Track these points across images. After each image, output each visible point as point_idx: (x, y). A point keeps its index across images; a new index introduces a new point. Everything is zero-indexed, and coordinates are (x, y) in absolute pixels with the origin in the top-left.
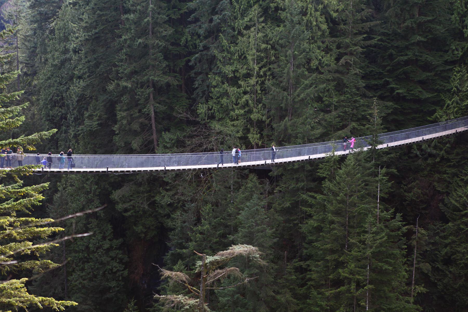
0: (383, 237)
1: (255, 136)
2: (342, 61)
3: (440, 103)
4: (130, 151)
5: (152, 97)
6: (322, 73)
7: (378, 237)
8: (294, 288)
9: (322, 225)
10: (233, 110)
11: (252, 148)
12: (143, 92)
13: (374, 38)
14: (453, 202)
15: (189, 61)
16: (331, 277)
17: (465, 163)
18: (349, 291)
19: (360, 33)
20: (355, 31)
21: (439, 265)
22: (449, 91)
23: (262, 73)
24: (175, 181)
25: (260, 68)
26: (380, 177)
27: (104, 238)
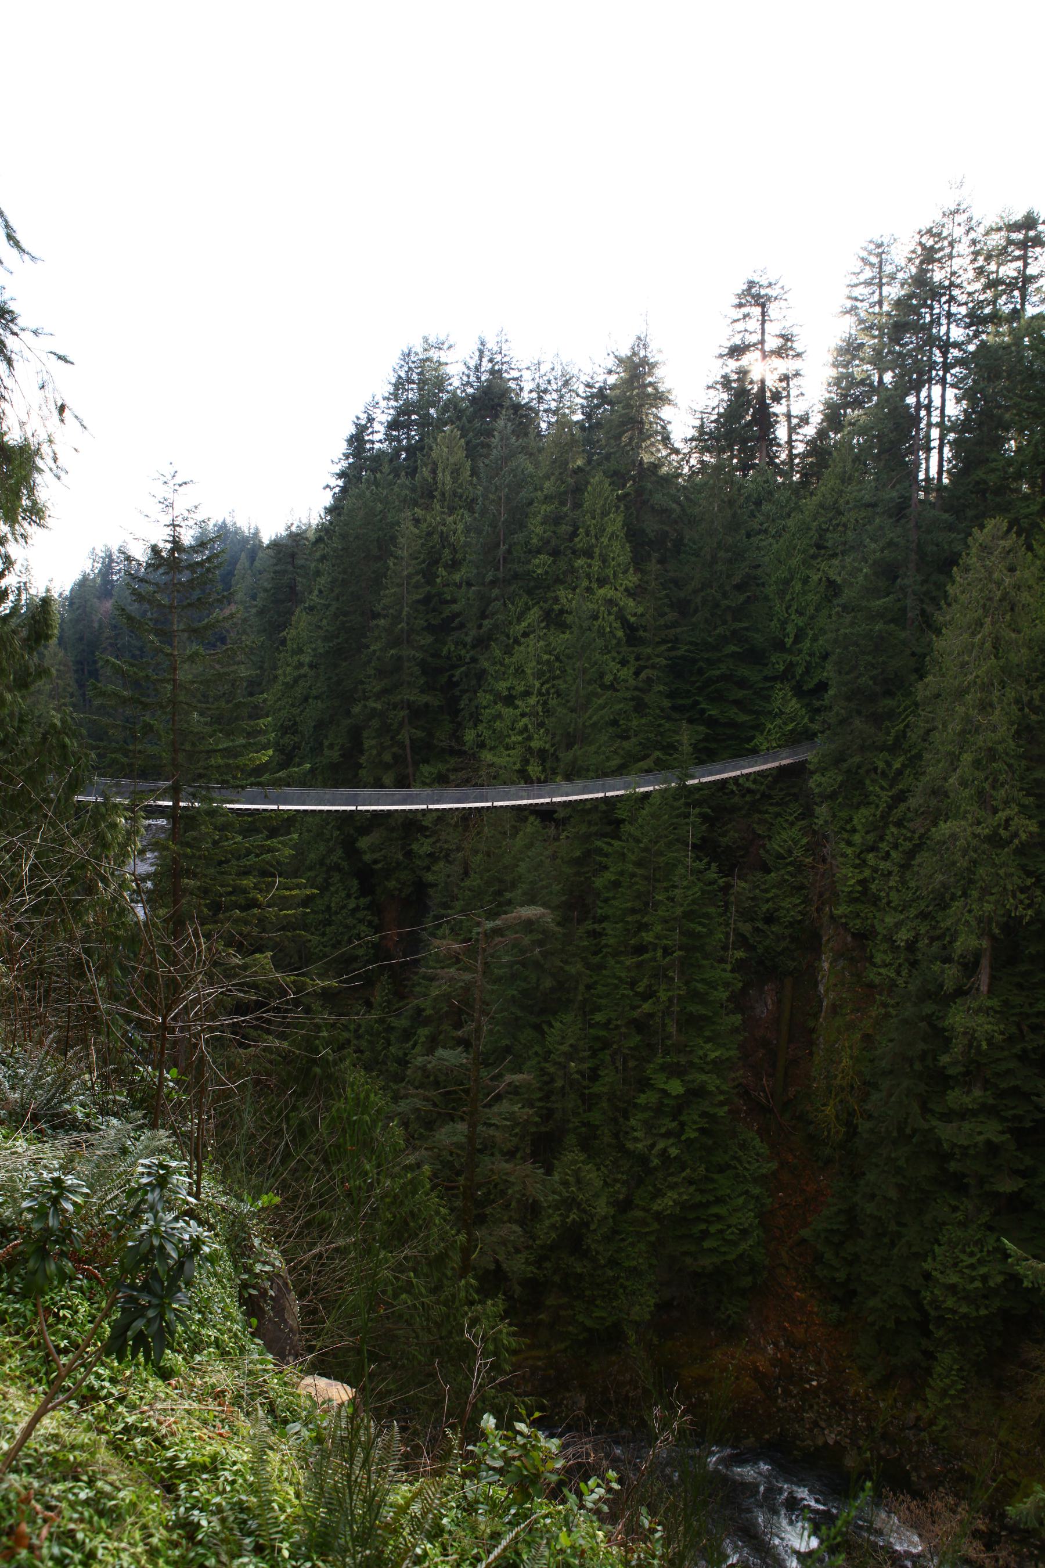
1: (536, 768)
2: (643, 676)
3: (759, 727)
4: (379, 784)
5: (406, 720)
6: (618, 691)
9: (621, 879)
10: (509, 736)
11: (532, 782)
12: (396, 715)
13: (679, 649)
14: (777, 847)
15: (453, 676)
16: (632, 942)
17: (790, 801)
18: (654, 959)
19: (664, 641)
20: (657, 639)
21: (759, 925)
22: (770, 713)
23: (544, 691)
24: (436, 825)
25: (542, 685)
26: (692, 819)
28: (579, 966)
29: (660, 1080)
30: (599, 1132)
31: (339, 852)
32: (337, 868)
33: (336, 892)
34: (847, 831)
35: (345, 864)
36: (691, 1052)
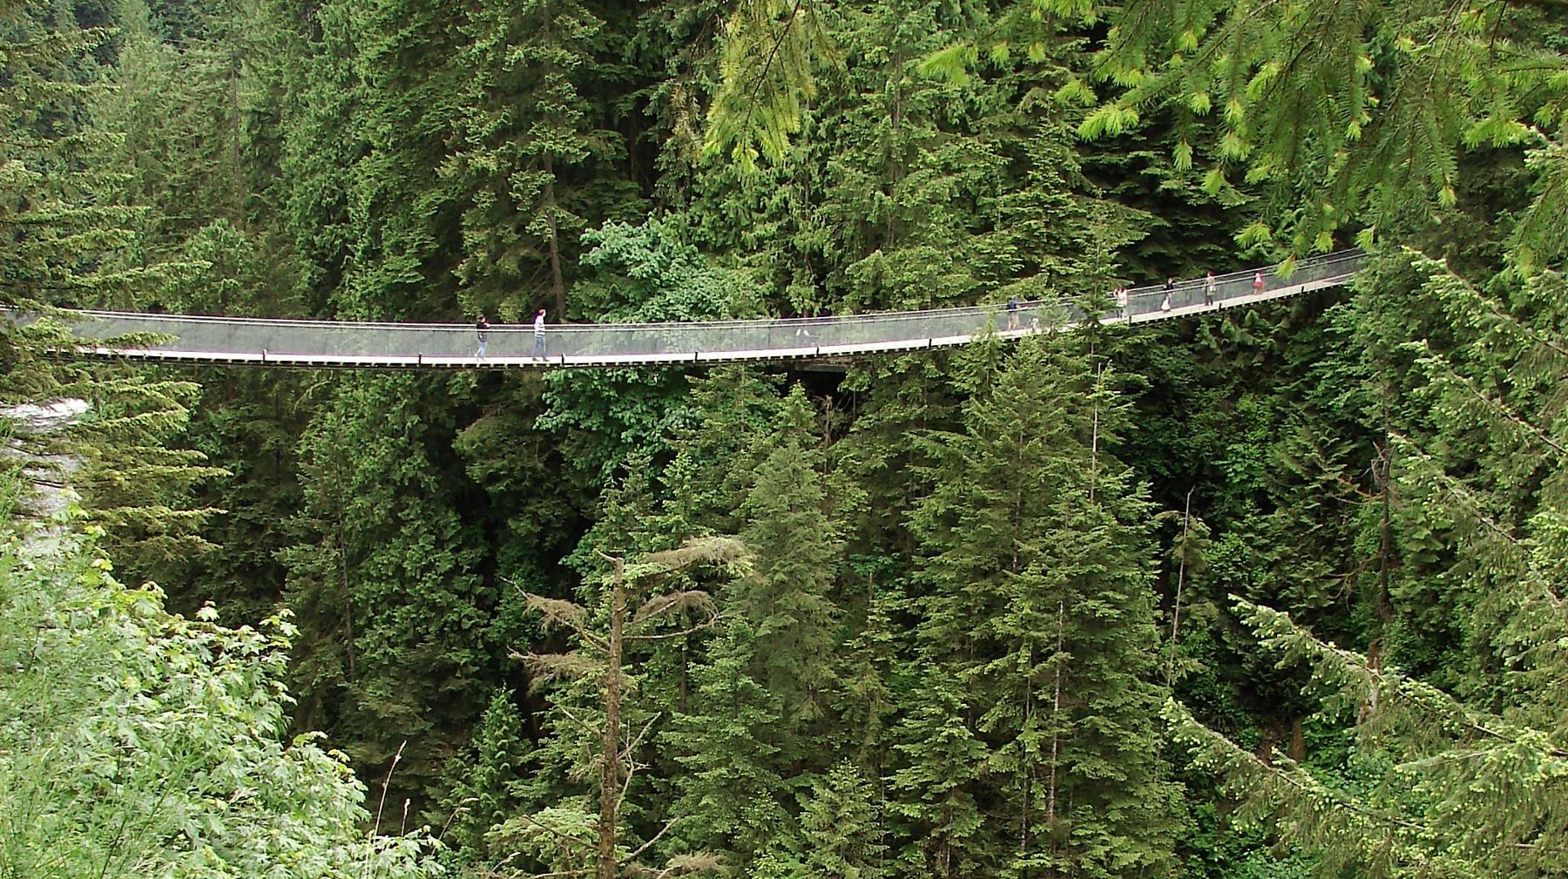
0: (1099, 538)
1: (802, 290)
2: (1025, 102)
5: (549, 190)
7: (1088, 538)
8: (886, 662)
10: (749, 228)
23: (822, 132)
25: (818, 120)
27: (440, 544)
31: (419, 458)
33: (414, 538)
34: (1422, 430)
36: (1082, 848)
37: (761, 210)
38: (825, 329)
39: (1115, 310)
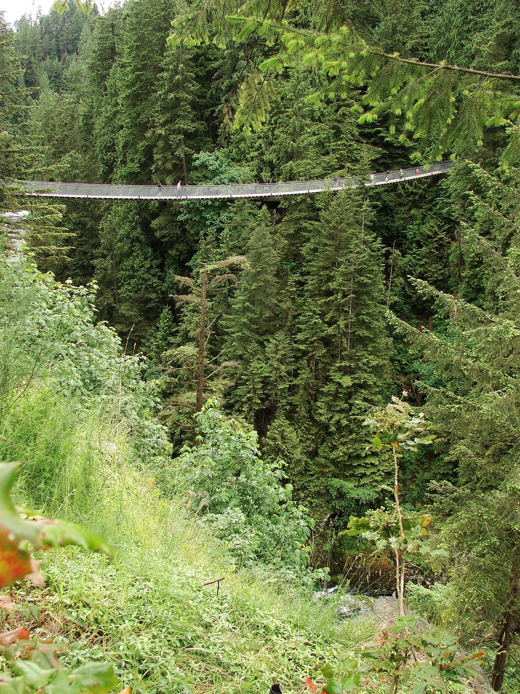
0: (365, 256)
5: (182, 141)
23: (273, 122)
25: (271, 118)
27: (146, 259)
28: (288, 303)
29: (337, 377)
30: (298, 409)
31: (139, 230)
32: (138, 240)
33: (137, 256)
35: (142, 237)
36: (359, 360)
37: (252, 148)
38: (274, 187)
39: (369, 181)
